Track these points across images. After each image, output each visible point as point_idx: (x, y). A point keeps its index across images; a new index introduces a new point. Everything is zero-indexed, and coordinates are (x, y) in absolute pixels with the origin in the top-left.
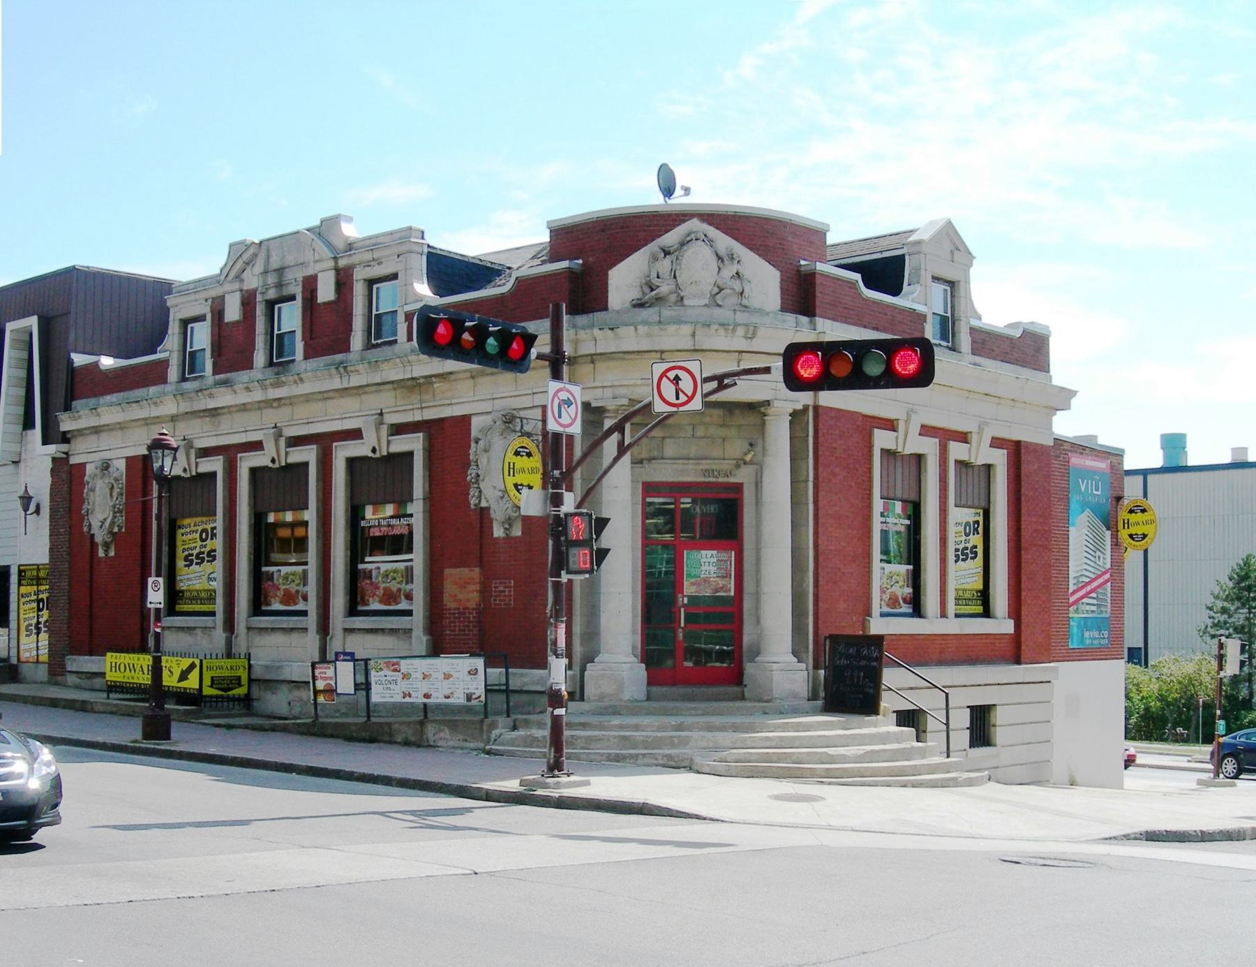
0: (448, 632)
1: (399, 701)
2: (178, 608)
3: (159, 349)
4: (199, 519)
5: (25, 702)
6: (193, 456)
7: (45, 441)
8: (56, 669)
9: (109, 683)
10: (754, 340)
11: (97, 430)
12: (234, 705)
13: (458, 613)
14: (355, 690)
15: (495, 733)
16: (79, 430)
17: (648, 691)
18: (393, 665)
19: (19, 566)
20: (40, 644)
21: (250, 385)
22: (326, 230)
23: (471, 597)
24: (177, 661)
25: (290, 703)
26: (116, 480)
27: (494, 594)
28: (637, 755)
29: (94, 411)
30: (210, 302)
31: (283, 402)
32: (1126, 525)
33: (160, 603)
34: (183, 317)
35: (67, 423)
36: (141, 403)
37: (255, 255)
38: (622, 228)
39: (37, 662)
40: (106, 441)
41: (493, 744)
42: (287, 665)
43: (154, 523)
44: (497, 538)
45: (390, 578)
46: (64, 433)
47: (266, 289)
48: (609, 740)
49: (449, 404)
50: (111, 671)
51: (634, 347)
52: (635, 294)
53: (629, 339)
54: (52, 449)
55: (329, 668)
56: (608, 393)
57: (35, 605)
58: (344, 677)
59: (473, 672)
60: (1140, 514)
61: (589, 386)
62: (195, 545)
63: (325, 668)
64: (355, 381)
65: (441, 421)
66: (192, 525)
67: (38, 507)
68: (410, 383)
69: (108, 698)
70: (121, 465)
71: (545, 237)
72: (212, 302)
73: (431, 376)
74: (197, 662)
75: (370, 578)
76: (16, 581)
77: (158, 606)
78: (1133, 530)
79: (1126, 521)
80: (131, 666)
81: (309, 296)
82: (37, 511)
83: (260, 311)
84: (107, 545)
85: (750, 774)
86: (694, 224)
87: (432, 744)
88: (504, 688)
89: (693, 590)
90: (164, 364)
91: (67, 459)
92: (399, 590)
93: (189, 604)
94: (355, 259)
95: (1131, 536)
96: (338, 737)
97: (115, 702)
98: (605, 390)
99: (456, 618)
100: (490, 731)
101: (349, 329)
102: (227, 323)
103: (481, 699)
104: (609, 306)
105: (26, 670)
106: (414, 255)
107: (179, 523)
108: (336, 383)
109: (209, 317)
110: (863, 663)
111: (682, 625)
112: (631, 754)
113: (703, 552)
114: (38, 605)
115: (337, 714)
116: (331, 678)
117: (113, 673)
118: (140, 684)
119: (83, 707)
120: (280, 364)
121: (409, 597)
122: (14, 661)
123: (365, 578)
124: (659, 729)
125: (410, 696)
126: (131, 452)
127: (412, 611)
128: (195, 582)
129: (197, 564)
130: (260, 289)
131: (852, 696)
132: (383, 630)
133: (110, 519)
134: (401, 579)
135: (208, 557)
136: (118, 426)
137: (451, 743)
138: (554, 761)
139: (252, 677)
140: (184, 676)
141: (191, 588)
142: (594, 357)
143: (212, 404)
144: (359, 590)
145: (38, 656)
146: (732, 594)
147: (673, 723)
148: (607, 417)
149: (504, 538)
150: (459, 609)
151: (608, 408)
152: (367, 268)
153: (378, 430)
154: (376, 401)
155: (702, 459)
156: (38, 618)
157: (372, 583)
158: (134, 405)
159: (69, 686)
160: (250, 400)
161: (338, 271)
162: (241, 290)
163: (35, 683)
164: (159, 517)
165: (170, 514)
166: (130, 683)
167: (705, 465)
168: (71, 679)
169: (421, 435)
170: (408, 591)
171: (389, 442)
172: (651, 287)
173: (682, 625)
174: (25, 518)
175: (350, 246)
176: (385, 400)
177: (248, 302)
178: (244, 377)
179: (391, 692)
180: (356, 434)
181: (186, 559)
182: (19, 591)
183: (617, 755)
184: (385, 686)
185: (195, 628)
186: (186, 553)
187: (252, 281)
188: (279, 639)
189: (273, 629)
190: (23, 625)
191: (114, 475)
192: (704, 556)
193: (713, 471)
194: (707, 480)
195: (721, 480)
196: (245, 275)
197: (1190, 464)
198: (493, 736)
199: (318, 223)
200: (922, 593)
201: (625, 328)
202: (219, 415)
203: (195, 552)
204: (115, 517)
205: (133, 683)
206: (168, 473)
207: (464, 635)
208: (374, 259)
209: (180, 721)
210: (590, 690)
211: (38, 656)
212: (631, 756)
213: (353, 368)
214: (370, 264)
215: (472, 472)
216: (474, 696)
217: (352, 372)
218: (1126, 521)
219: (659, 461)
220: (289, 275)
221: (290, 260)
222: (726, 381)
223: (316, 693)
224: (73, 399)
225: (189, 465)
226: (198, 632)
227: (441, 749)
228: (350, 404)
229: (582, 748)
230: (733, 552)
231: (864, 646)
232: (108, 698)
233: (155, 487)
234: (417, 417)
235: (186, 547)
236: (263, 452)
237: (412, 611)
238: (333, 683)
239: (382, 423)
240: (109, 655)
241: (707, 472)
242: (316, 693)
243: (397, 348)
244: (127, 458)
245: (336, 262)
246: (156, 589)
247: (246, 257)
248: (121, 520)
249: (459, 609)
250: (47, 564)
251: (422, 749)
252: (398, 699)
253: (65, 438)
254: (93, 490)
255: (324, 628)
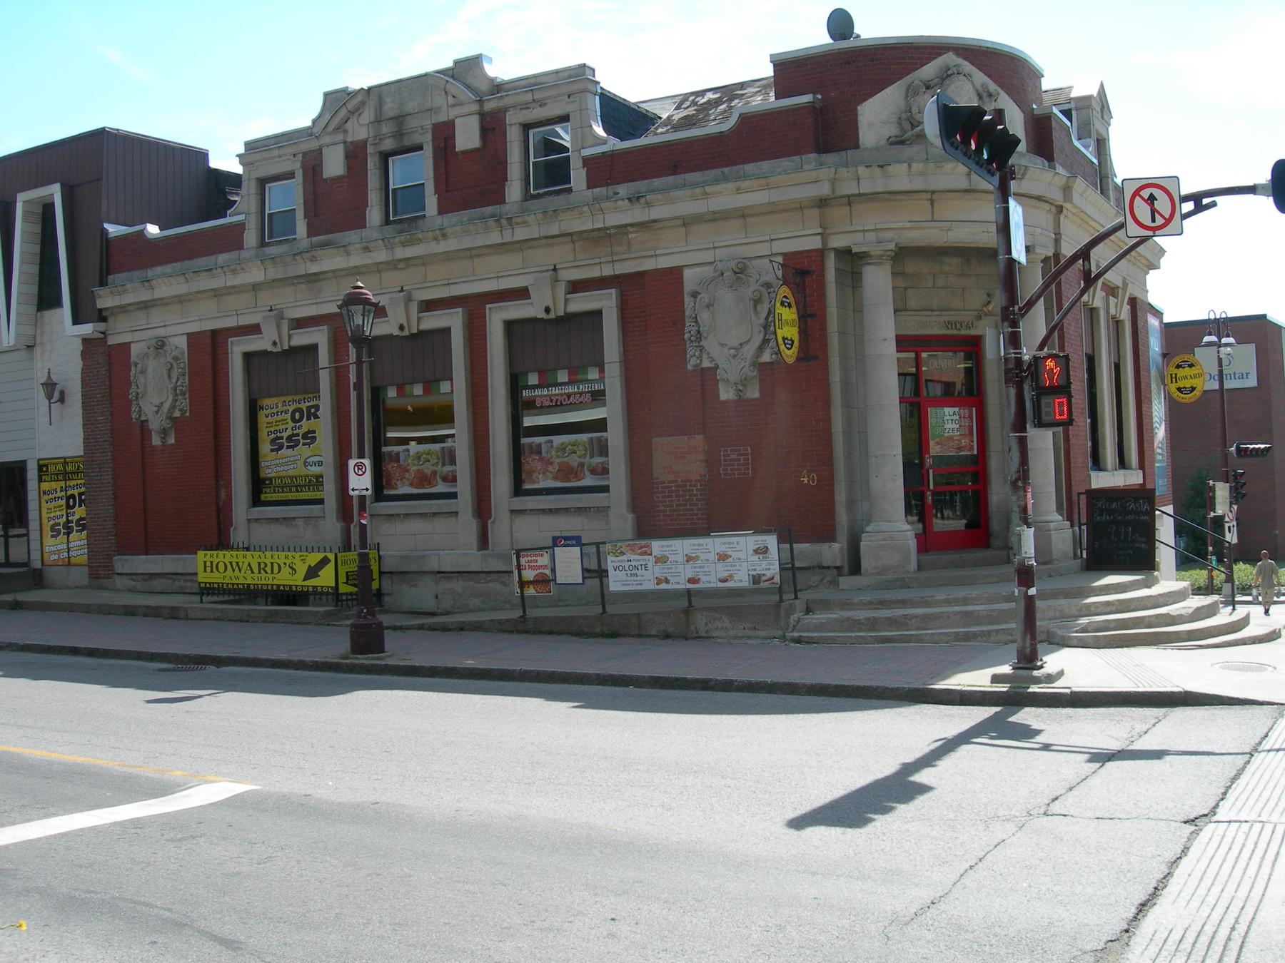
0: (662, 508)
1: (653, 588)
2: (263, 497)
3: (229, 212)
4: (290, 398)
5: (88, 612)
6: (285, 329)
7: (76, 321)
8: (100, 570)
9: (203, 585)
10: (1024, 180)
11: (145, 306)
12: (327, 599)
13: (676, 486)
14: (584, 578)
15: (794, 617)
16: (121, 307)
17: (918, 560)
18: (641, 547)
19: (39, 460)
20: (71, 545)
21: (371, 245)
22: (468, 68)
23: (694, 467)
24: (300, 556)
25: (437, 597)
26: (176, 358)
27: (723, 463)
28: (989, 632)
29: (146, 284)
30: (300, 157)
31: (412, 262)
32: (1174, 380)
33: (367, 489)
34: (258, 176)
35: (106, 300)
36: (214, 271)
37: (363, 103)
38: (872, 60)
39: (69, 564)
40: (157, 316)
41: (792, 632)
42: (432, 554)
43: (353, 395)
44: (727, 402)
45: (422, 459)
46: (100, 311)
47: (380, 139)
48: (949, 617)
49: (652, 256)
50: (205, 571)
51: (904, 185)
52: (892, 130)
53: (871, 181)
54: (87, 329)
55: (542, 555)
56: (871, 237)
57: (63, 502)
58: (569, 565)
59: (762, 551)
60: (1187, 369)
61: (846, 230)
62: (284, 427)
63: (536, 556)
64: (521, 234)
65: (641, 275)
66: (280, 405)
67: (62, 394)
68: (596, 234)
69: (202, 602)
70: (183, 343)
71: (768, 71)
72: (303, 158)
73: (626, 226)
74: (331, 556)
75: (398, 460)
76: (36, 477)
77: (364, 493)
78: (1181, 384)
79: (1174, 376)
80: (234, 565)
81: (442, 145)
82: (62, 399)
83: (372, 164)
84: (164, 432)
85: (1081, 644)
86: (950, 58)
87: (704, 634)
88: (790, 566)
89: (938, 450)
90: (240, 227)
91: (104, 340)
92: (435, 473)
93: (279, 492)
94: (507, 101)
95: (1179, 389)
96: (560, 633)
97: (211, 606)
98: (866, 234)
99: (672, 492)
100: (788, 616)
101: (503, 178)
102: (326, 180)
103: (775, 580)
104: (860, 142)
105: (51, 574)
106: (588, 94)
107: (259, 403)
108: (495, 238)
109: (299, 174)
110: (1130, 517)
111: (932, 487)
112: (983, 631)
113: (945, 409)
114: (68, 503)
115: (507, 606)
116: (545, 567)
117: (208, 574)
118: (249, 585)
119: (173, 614)
120: (400, 221)
121: (452, 479)
122: (37, 564)
123: (391, 460)
124: (991, 601)
125: (667, 581)
126: (195, 328)
127: (456, 493)
128: (286, 468)
129: (288, 447)
130: (371, 141)
131: (1120, 552)
132: (567, 510)
133: (170, 401)
134: (436, 461)
135: (303, 438)
136: (143, 305)
137: (732, 633)
138: (1031, 651)
139: (382, 570)
140: (312, 572)
141: (282, 474)
142: (851, 198)
143: (314, 268)
144: (384, 474)
145: (69, 557)
146: (975, 453)
147: (1004, 594)
148: (870, 264)
149: (734, 401)
150: (676, 481)
151: (872, 253)
152: (524, 111)
153: (553, 287)
154: (544, 257)
155: (946, 310)
156: (67, 516)
157: (399, 466)
158: (204, 274)
159: (118, 590)
160: (370, 261)
161: (483, 115)
162: (345, 142)
163: (68, 587)
164: (358, 386)
165: (372, 379)
166: (233, 584)
167: (948, 317)
168: (119, 582)
169: (613, 291)
170: (444, 473)
171: (419, 319)
172: (912, 124)
173: (932, 487)
174: (50, 407)
175: (498, 87)
176: (559, 254)
177: (355, 154)
178: (354, 237)
179: (639, 578)
180: (255, 329)
181: (273, 441)
182: (39, 488)
183: (966, 634)
184: (629, 572)
185: (294, 518)
186: (273, 436)
187: (359, 130)
188: (417, 525)
189: (407, 515)
190: (47, 528)
191: (174, 354)
192: (947, 414)
193: (955, 323)
194: (949, 332)
195: (963, 332)
196: (349, 126)
197: (559, 381)
198: (792, 622)
199: (451, 64)
200: (1100, 444)
201: (898, 165)
202: (319, 280)
203: (285, 435)
204: (176, 401)
205: (238, 584)
206: (368, 334)
207: (687, 510)
208: (534, 100)
209: (320, 624)
210: (866, 564)
211: (69, 557)
212: (982, 634)
213: (519, 220)
214: (528, 106)
215: (133, 390)
216: (764, 578)
217: (517, 224)
218: (1174, 376)
219: (903, 313)
220: (413, 123)
221: (411, 106)
222: (1205, 201)
223: (523, 584)
224: (108, 274)
225: (280, 337)
226: (300, 523)
227: (719, 640)
228: (511, 261)
229: (918, 629)
230: (974, 409)
231: (1129, 501)
232: (202, 602)
233: (352, 352)
234: (607, 271)
235: (272, 429)
236: (529, 301)
237: (456, 493)
238: (548, 572)
239: (557, 281)
240: (201, 554)
241: (949, 324)
242: (523, 584)
243: (572, 197)
244: (188, 334)
245: (481, 106)
246: (360, 473)
247: (350, 106)
248: (184, 403)
249: (676, 481)
250: (82, 456)
251: (690, 642)
252: (650, 585)
253: (101, 317)
254: (143, 372)
255: (483, 509)
